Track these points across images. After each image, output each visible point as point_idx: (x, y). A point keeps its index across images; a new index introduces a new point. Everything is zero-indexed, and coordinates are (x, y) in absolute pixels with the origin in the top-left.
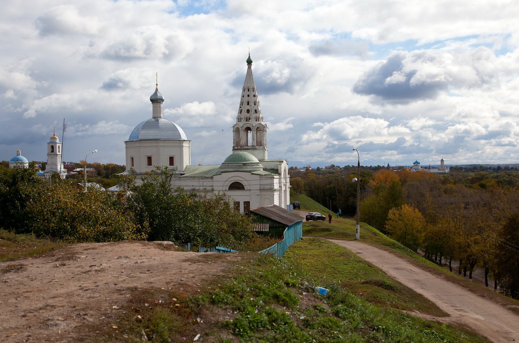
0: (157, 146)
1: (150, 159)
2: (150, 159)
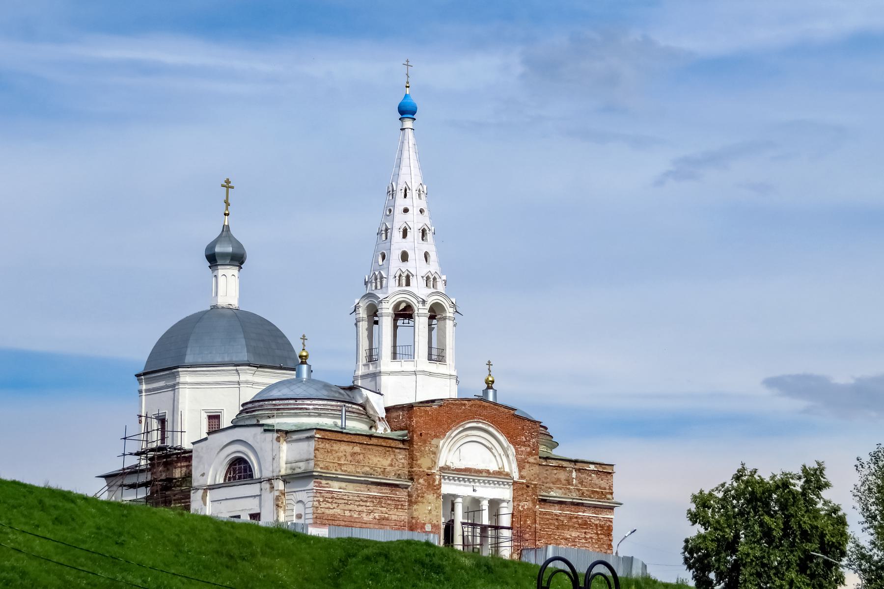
0: (174, 385)
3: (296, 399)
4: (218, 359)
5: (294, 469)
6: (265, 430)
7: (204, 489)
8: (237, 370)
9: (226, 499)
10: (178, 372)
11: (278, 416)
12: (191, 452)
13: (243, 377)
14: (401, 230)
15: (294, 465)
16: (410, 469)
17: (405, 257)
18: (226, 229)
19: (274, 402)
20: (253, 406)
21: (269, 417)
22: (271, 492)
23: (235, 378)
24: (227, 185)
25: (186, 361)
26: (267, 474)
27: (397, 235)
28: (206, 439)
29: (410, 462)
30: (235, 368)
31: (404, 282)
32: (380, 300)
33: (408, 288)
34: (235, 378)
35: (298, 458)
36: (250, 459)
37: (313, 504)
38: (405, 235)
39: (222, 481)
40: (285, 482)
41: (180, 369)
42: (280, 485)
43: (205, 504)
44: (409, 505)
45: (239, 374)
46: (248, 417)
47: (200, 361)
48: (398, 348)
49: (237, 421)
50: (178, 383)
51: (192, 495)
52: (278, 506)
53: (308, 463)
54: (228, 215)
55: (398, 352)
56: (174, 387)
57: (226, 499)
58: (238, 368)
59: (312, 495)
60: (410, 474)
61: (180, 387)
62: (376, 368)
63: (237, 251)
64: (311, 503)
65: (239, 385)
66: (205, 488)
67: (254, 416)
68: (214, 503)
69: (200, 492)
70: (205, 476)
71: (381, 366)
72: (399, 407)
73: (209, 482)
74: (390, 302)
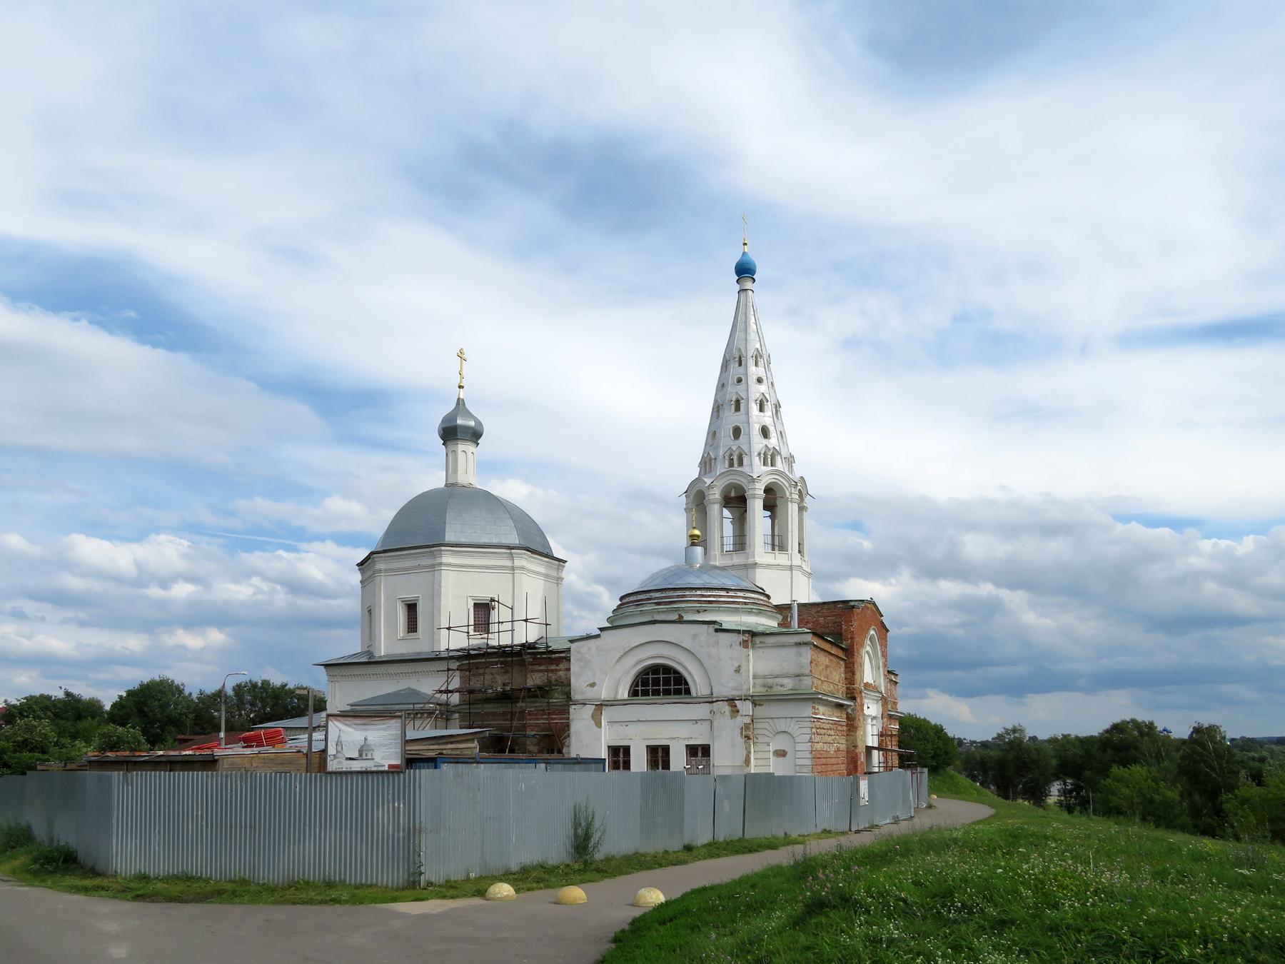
0: (433, 566)
1: (412, 608)
2: (412, 608)
3: (727, 590)
4: (485, 540)
5: (771, 687)
6: (717, 631)
7: (596, 705)
8: (511, 553)
9: (639, 721)
10: (441, 551)
11: (712, 611)
12: (568, 650)
13: (517, 563)
14: (758, 402)
15: (770, 681)
16: (849, 686)
17: (765, 432)
18: (460, 402)
19: (699, 592)
20: (663, 595)
21: (699, 612)
22: (732, 717)
23: (508, 563)
24: (461, 355)
25: (446, 540)
26: (726, 688)
27: (754, 408)
28: (598, 636)
29: (848, 677)
30: (509, 551)
31: (736, 462)
32: (707, 485)
33: (740, 469)
34: (508, 563)
35: (777, 671)
36: (686, 669)
37: (811, 738)
38: (761, 410)
39: (626, 696)
40: (755, 704)
41: (443, 548)
42: (746, 708)
43: (599, 725)
44: (849, 730)
45: (513, 557)
46: (665, 610)
47: (463, 540)
48: (725, 539)
49: (615, 619)
50: (441, 564)
51: (571, 710)
52: (748, 737)
53: (800, 680)
54: (463, 387)
55: (725, 543)
56: (434, 568)
57: (639, 721)
58: (513, 551)
59: (809, 725)
60: (849, 691)
61: (443, 568)
62: (748, 558)
63: (477, 428)
64: (808, 737)
65: (514, 570)
66: (599, 703)
67: (677, 610)
68: (614, 725)
69: (589, 709)
70: (595, 688)
71: (756, 557)
72: (785, 606)
73: (605, 694)
74: (763, 482)
